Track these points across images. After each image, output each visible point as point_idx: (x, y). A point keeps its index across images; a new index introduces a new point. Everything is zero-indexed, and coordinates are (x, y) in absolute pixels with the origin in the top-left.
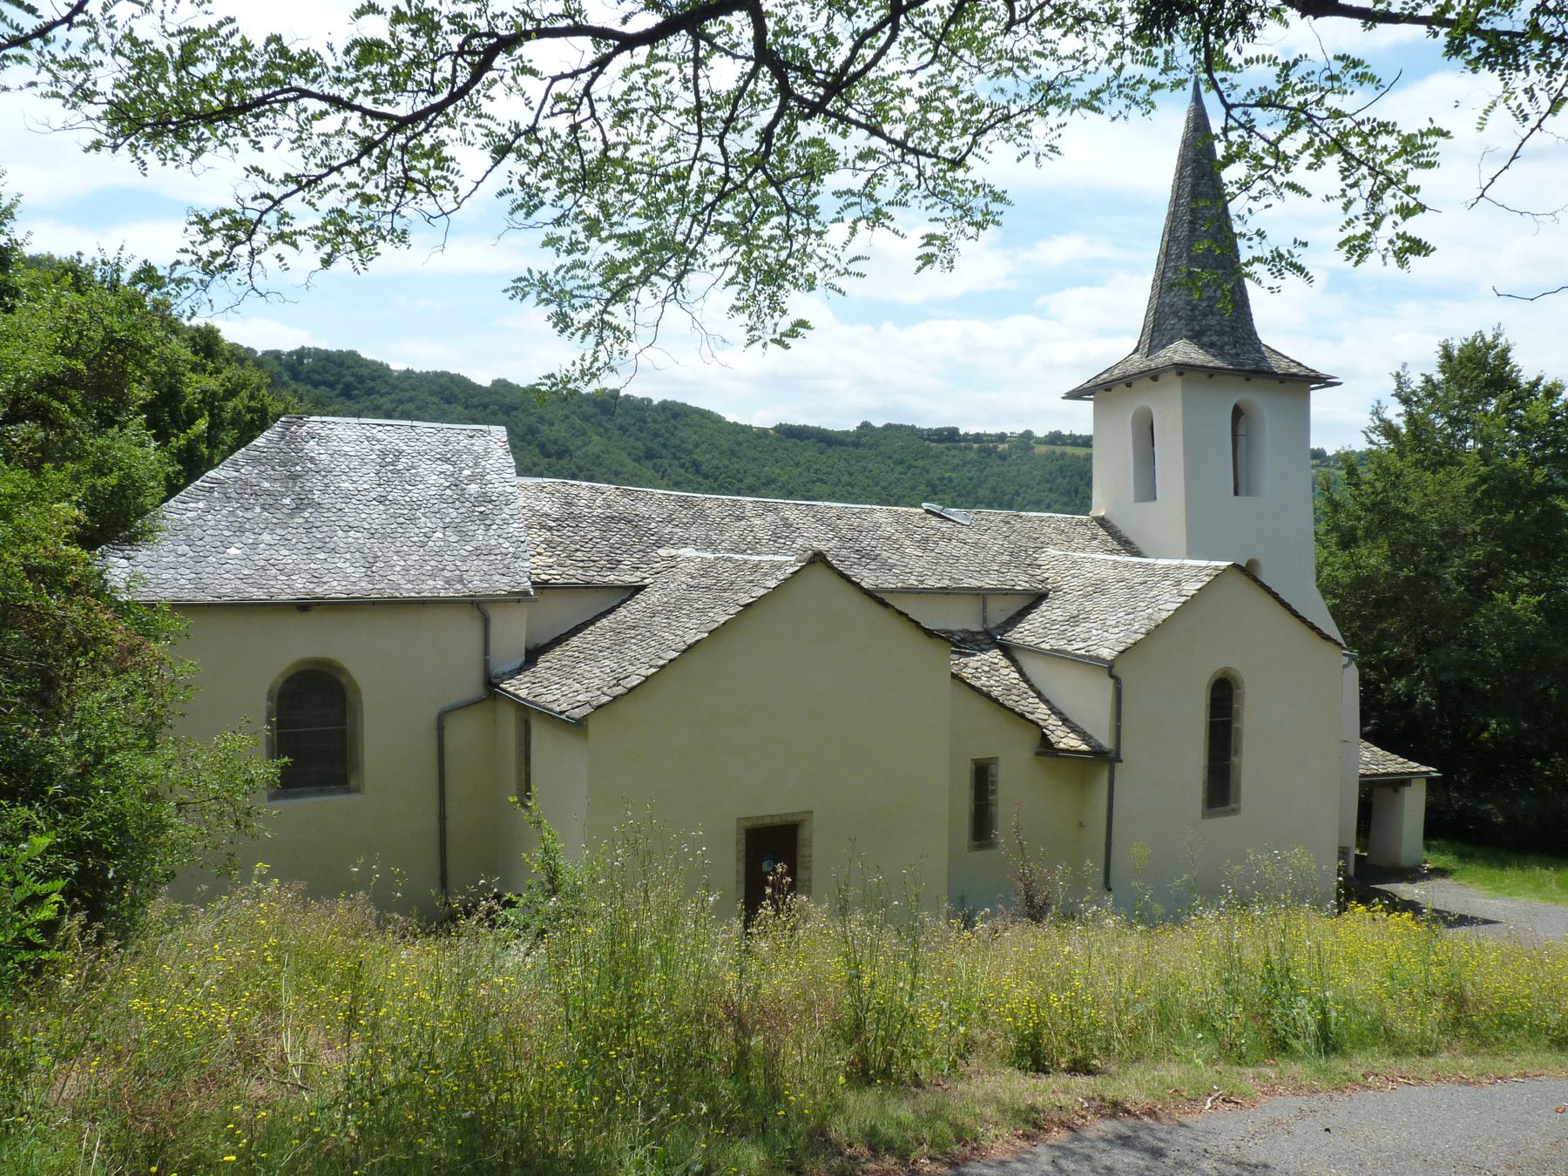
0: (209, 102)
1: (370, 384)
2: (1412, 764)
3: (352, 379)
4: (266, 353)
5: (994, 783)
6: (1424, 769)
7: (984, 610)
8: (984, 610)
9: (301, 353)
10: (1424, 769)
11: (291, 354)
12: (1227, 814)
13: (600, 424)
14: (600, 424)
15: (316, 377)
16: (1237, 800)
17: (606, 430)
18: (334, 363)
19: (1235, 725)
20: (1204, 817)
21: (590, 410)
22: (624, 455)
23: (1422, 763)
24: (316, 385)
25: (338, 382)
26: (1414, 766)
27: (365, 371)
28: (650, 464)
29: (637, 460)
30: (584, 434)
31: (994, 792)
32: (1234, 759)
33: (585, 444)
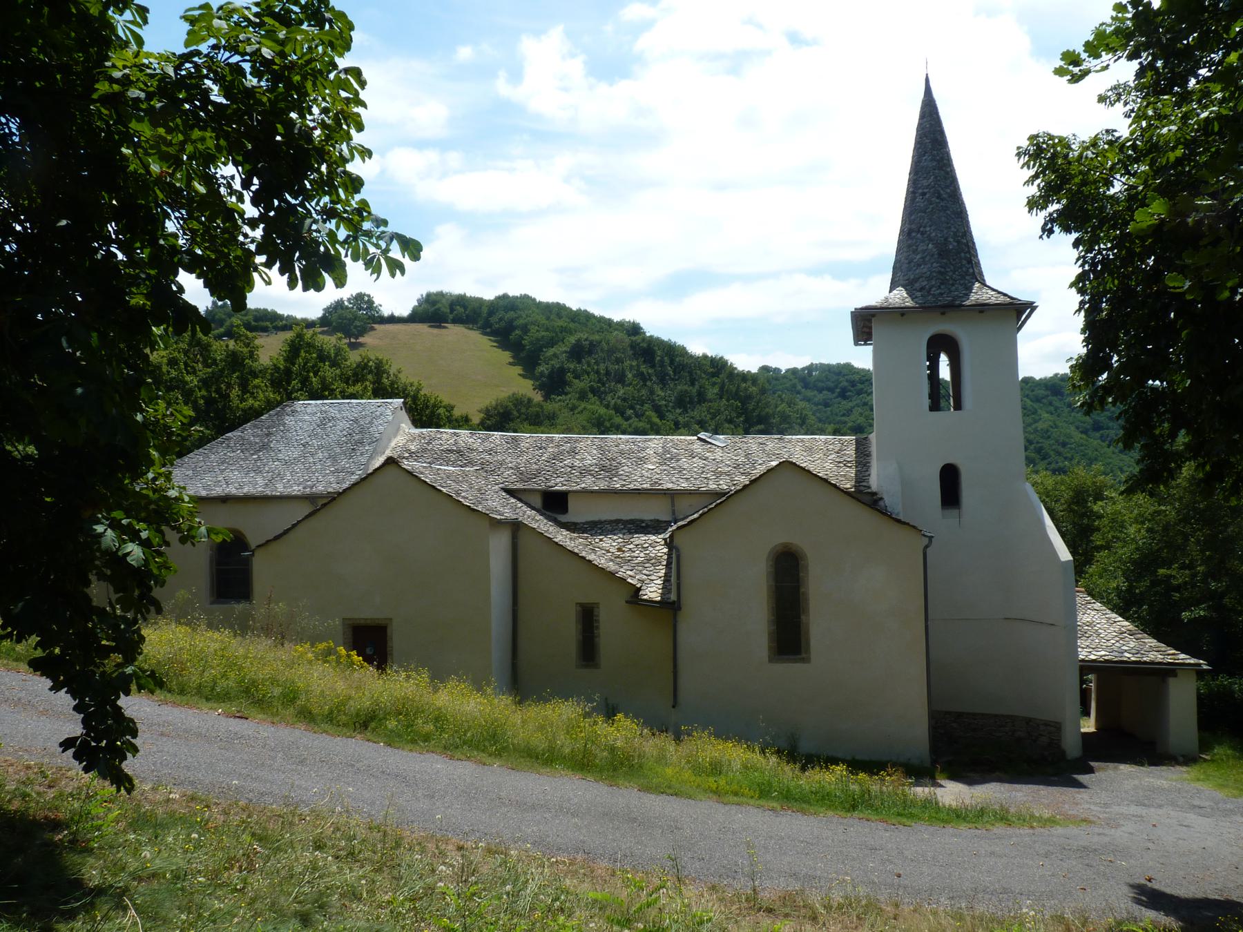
0: (116, 256)
1: (860, 386)
2: (1182, 656)
3: (845, 384)
4: (787, 371)
5: (598, 621)
6: (1192, 661)
7: (673, 505)
8: (673, 505)
9: (811, 368)
10: (1192, 661)
11: (803, 369)
12: (795, 661)
13: (1051, 404)
14: (1051, 404)
15: (820, 384)
16: (808, 651)
17: (1056, 409)
18: (835, 373)
19: (802, 590)
20: (770, 661)
21: (1042, 392)
22: (1073, 428)
23: (1193, 656)
24: (820, 391)
25: (836, 387)
26: (1183, 657)
27: (856, 377)
28: (1098, 435)
29: (1085, 432)
30: (1035, 412)
31: (598, 628)
32: (803, 617)
33: (1036, 421)
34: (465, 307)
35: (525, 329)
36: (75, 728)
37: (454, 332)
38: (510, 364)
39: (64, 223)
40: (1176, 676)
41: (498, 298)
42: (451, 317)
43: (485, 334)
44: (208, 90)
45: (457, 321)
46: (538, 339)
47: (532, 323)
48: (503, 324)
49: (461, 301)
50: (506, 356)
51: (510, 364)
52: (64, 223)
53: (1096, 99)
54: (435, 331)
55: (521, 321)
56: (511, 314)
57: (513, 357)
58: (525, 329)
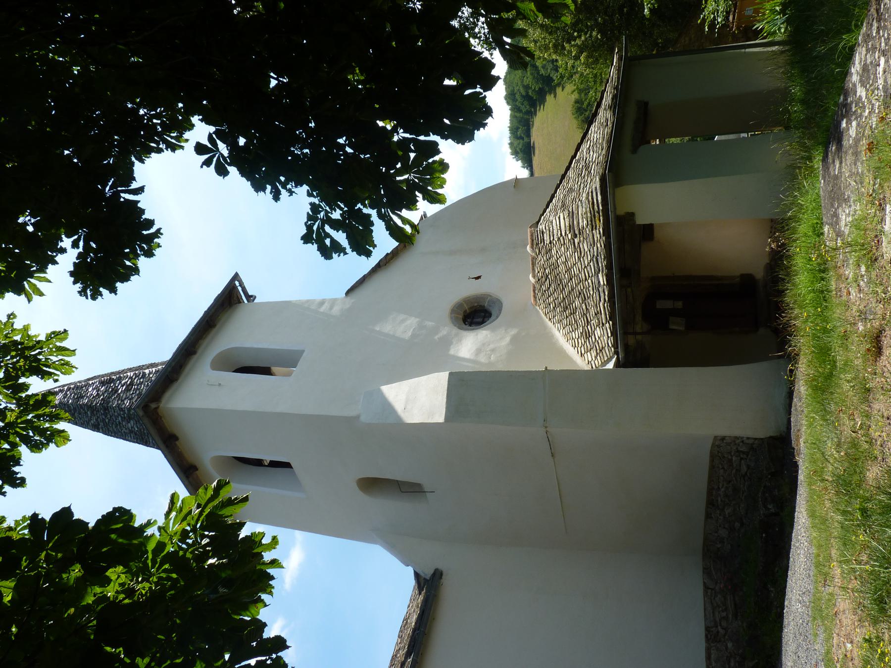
34: (518, 128)
35: (527, 87)
36: (139, 205)
37: (537, 136)
38: (555, 96)
39: (447, 121)
40: (632, 215)
41: (508, 103)
42: (526, 140)
43: (535, 114)
44: (387, 134)
45: (528, 134)
46: (534, 78)
47: (522, 82)
48: (526, 103)
49: (513, 130)
50: (550, 98)
51: (555, 96)
52: (447, 121)
53: (440, 567)
54: (537, 152)
55: (522, 90)
56: (518, 96)
57: (550, 94)
58: (527, 87)
